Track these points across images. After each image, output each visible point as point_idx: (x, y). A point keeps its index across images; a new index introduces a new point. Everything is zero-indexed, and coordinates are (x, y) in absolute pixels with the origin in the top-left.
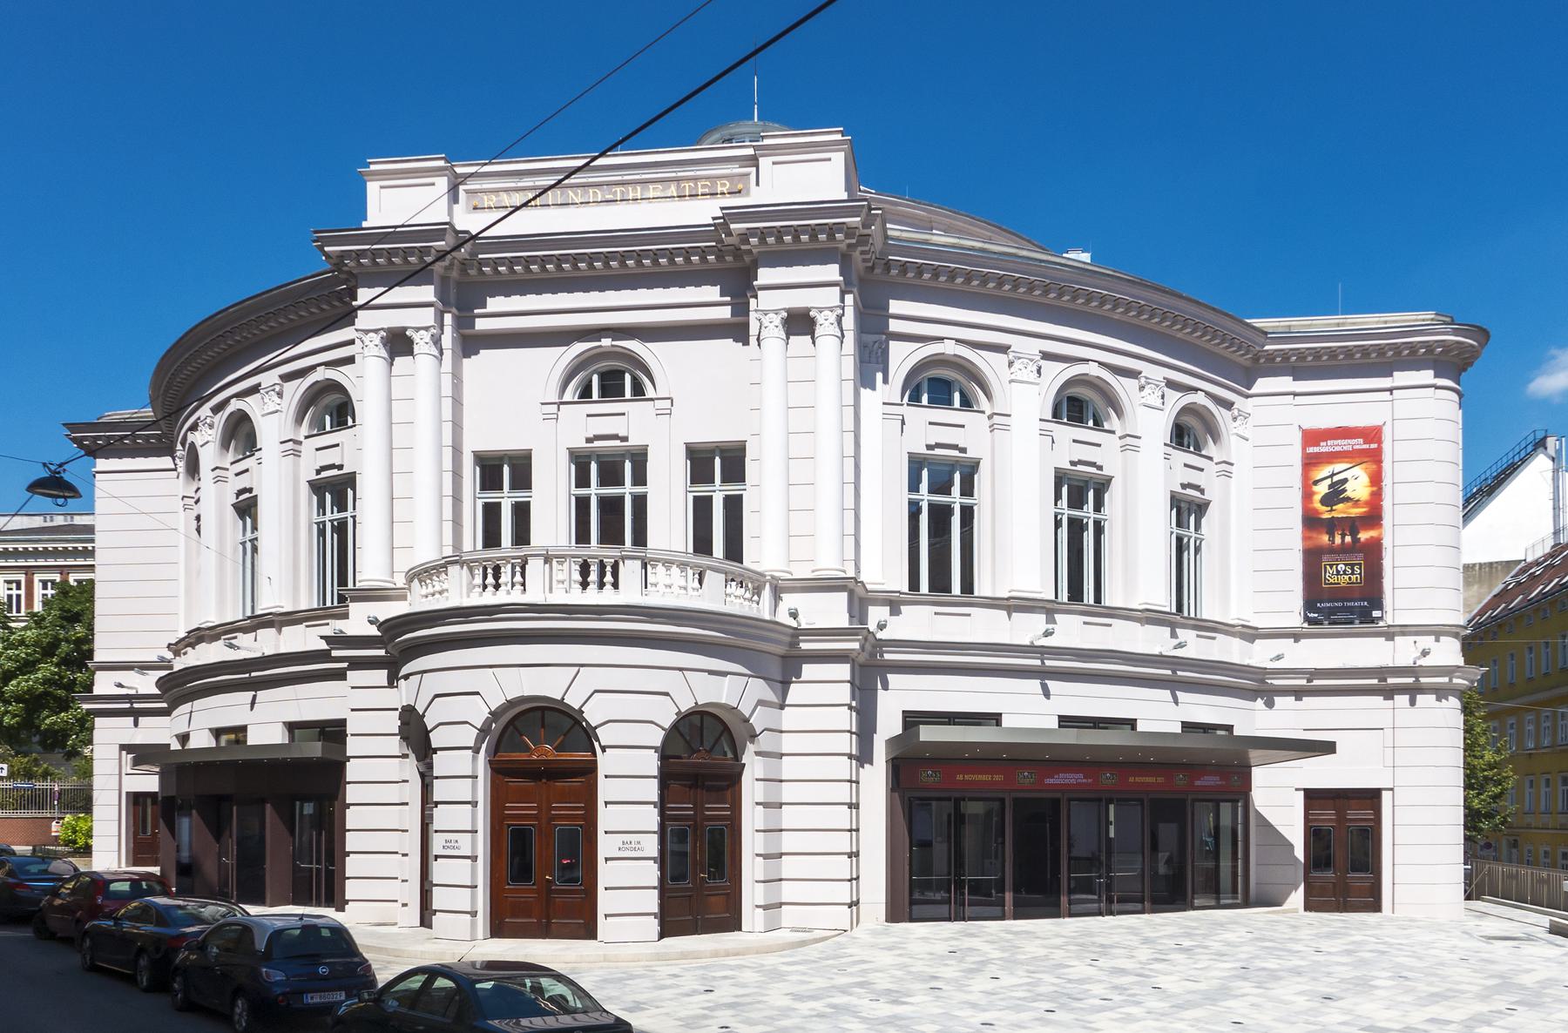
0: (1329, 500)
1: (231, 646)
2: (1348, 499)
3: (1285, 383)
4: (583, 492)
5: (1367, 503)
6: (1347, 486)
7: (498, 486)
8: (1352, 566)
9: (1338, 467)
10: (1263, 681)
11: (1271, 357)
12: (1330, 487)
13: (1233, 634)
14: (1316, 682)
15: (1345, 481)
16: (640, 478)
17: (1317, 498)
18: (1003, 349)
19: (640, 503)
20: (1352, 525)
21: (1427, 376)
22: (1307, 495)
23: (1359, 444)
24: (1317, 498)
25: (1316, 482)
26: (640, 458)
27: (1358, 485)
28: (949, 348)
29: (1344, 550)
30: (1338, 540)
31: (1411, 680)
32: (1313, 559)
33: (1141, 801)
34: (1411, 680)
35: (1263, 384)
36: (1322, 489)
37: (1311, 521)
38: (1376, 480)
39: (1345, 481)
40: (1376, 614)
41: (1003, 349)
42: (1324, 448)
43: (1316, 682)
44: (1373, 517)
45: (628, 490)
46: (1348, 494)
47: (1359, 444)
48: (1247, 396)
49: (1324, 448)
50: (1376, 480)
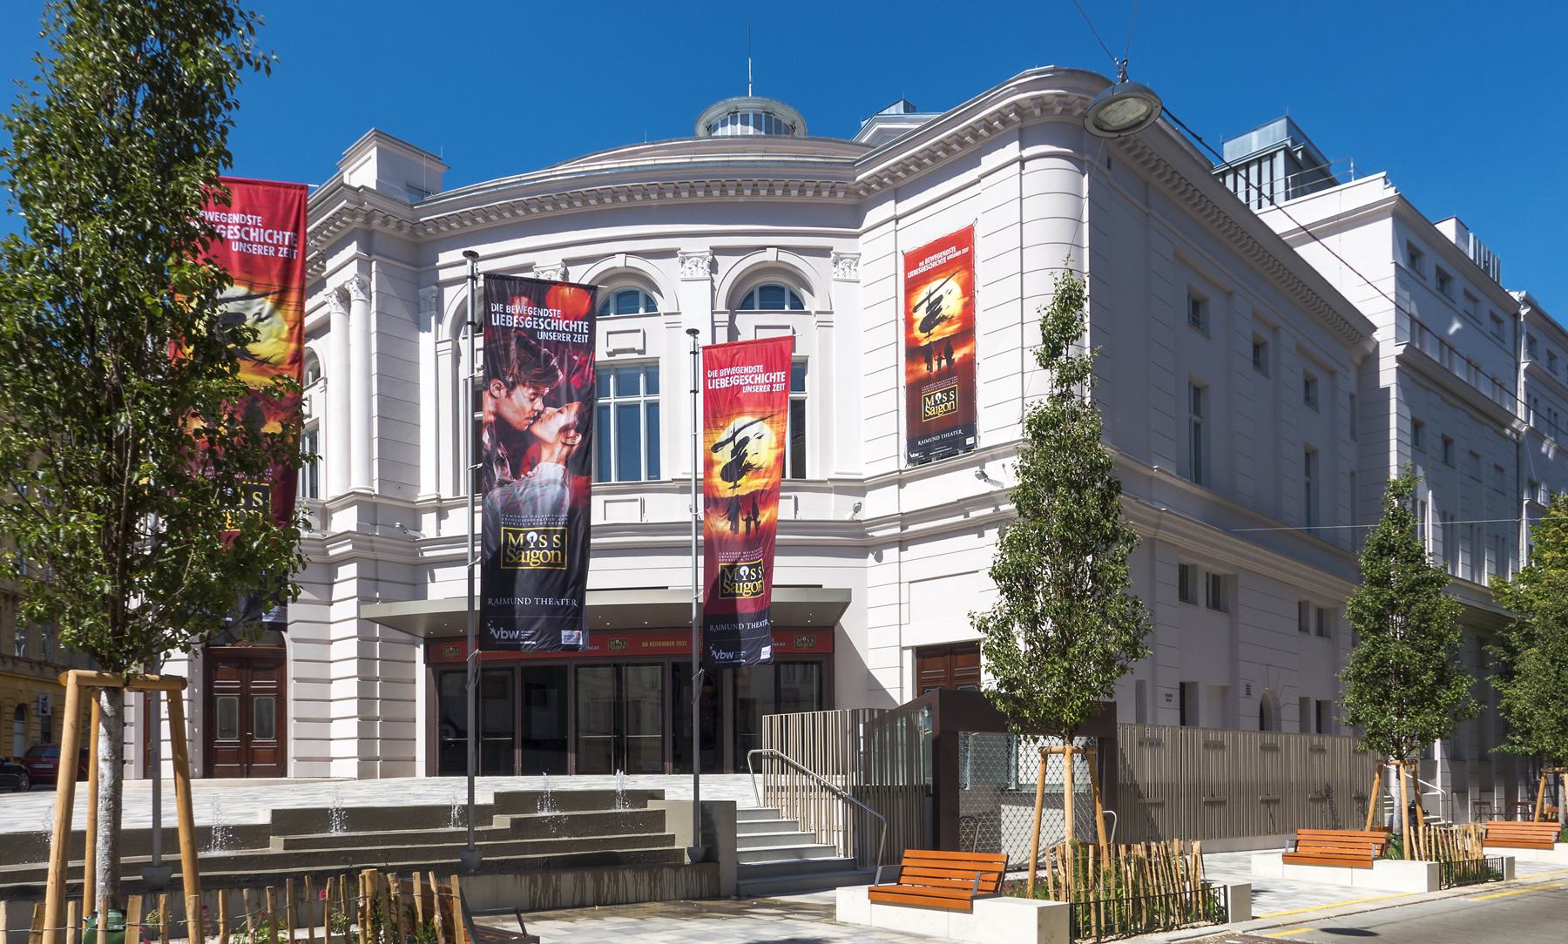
0: (927, 326)
1: (983, 476)
2: (944, 318)
3: (887, 209)
4: (652, 398)
5: (959, 318)
6: (943, 304)
7: (621, 408)
8: (948, 392)
9: (934, 285)
10: (864, 535)
11: (866, 185)
12: (928, 309)
13: (829, 490)
14: (912, 528)
15: (941, 297)
16: (653, 388)
17: (917, 325)
18: (670, 253)
19: (653, 408)
20: (947, 346)
21: (1012, 150)
22: (909, 322)
23: (952, 253)
24: (917, 325)
25: (915, 310)
26: (651, 370)
27: (952, 305)
28: (618, 262)
29: (942, 375)
30: (935, 367)
31: (990, 511)
32: (915, 391)
33: (662, 664)
34: (990, 511)
35: (872, 217)
36: (921, 314)
37: (915, 353)
38: (968, 289)
39: (941, 297)
40: (970, 441)
41: (670, 253)
42: (923, 267)
43: (912, 528)
44: (966, 333)
45: (642, 398)
46: (944, 312)
47: (952, 253)
48: (857, 236)
49: (923, 267)
50: (968, 289)
